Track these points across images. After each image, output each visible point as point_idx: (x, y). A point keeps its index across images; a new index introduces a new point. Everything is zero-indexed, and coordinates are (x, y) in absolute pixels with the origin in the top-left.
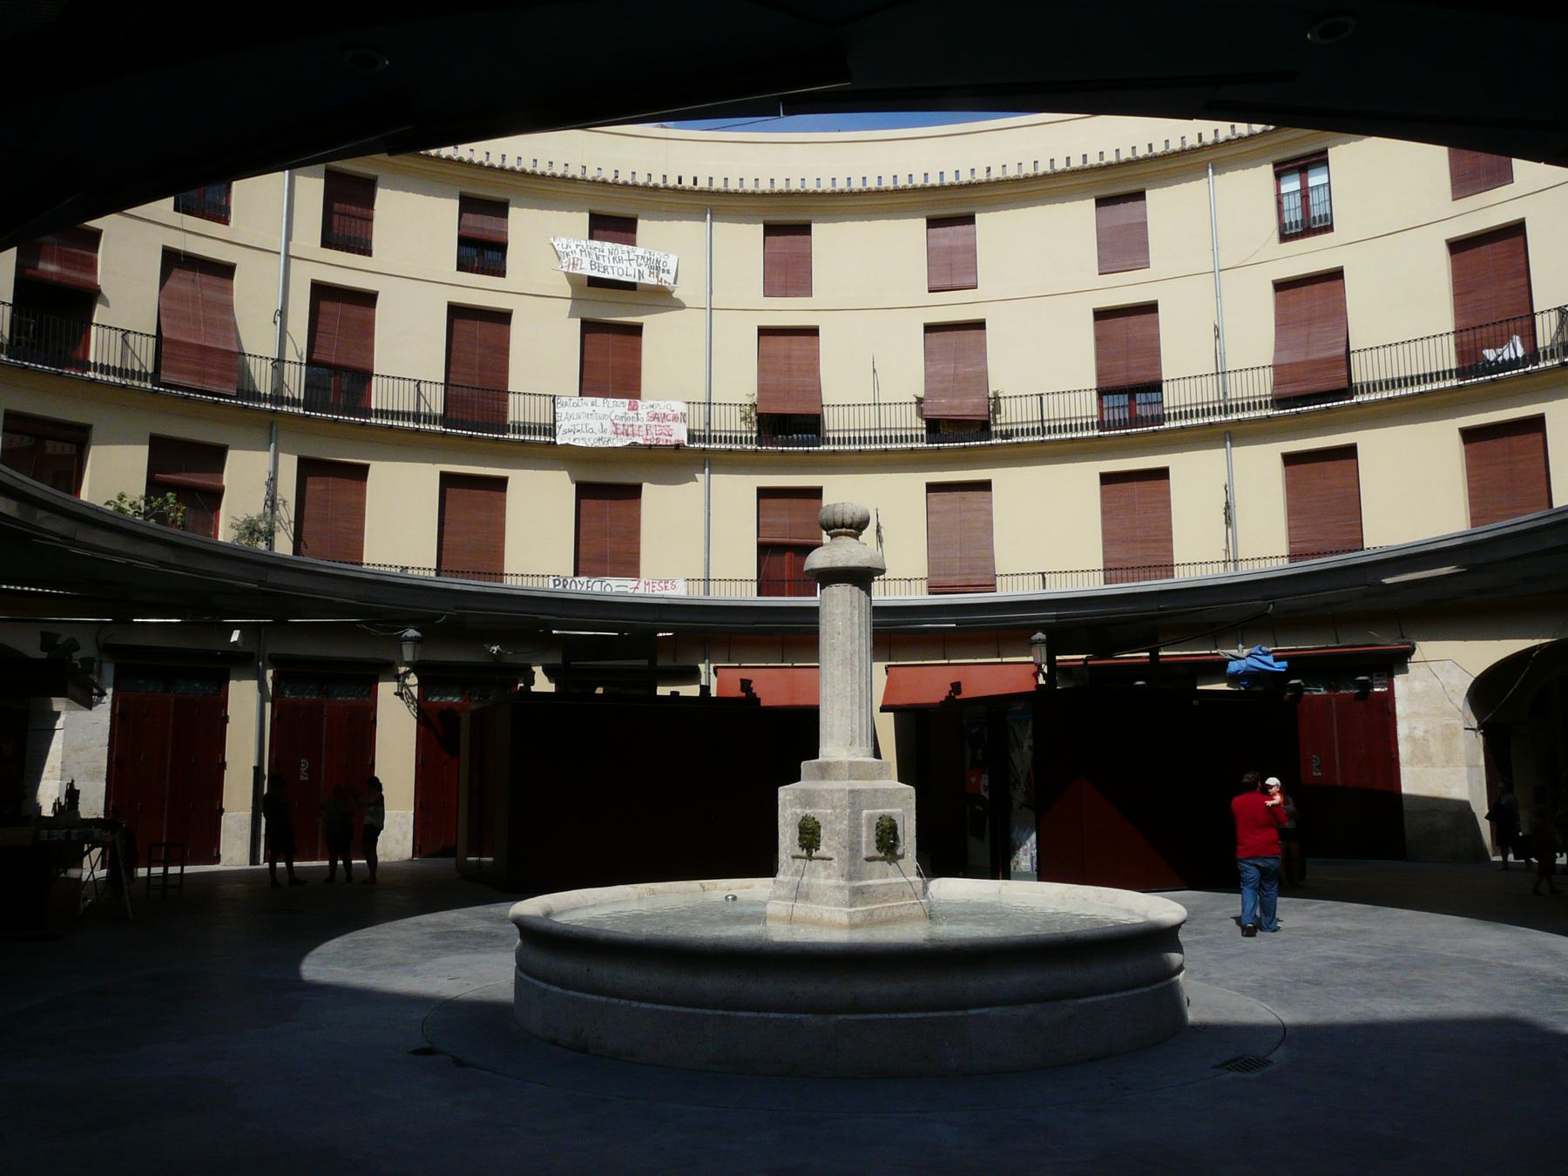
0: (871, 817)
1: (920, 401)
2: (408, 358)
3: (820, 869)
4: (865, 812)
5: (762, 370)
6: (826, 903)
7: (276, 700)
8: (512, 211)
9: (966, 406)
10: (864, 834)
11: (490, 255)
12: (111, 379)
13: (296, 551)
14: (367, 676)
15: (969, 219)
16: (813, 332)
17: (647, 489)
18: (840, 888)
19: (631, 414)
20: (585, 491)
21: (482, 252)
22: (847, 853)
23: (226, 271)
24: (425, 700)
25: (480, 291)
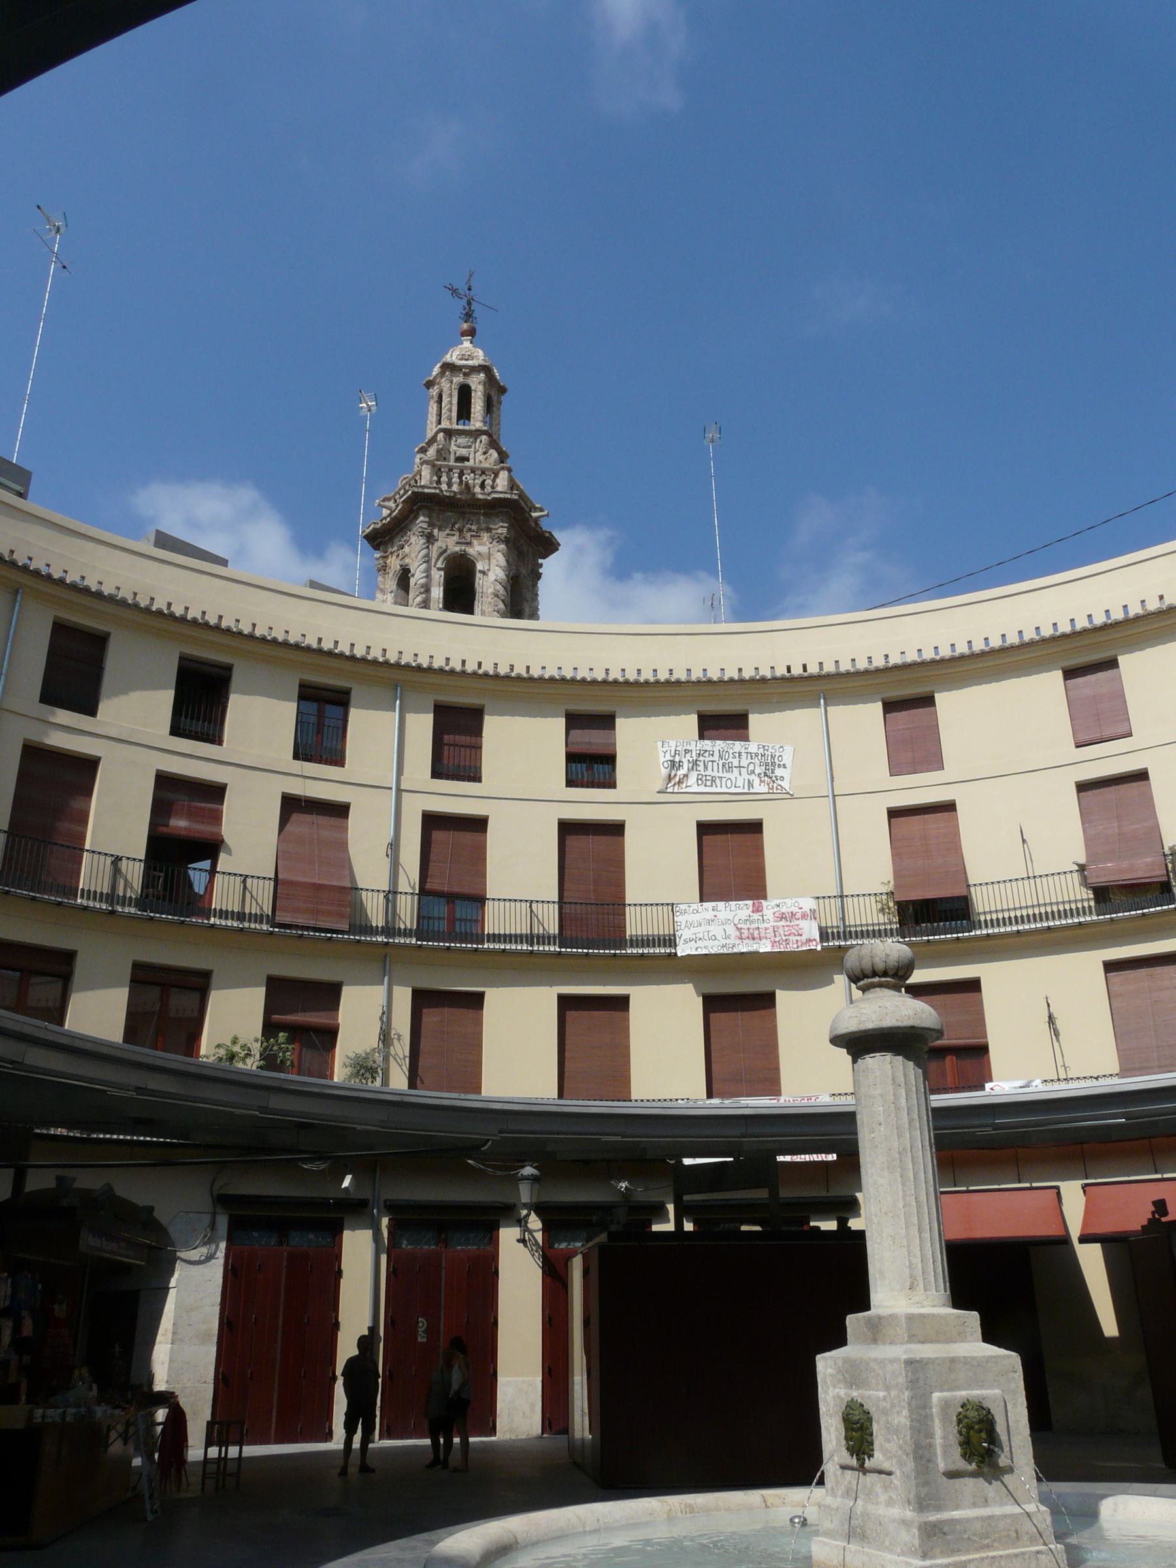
0: (946, 1405)
1: (1082, 868)
2: (521, 879)
3: (878, 1488)
4: (936, 1396)
5: (896, 854)
6: (891, 1551)
7: (392, 1250)
8: (619, 722)
9: (1143, 867)
10: (938, 1433)
11: (599, 768)
12: (229, 923)
13: (412, 1085)
14: (487, 1221)
15: (1112, 664)
16: (949, 807)
17: (781, 996)
18: (904, 1522)
19: (756, 916)
20: (713, 1004)
21: (591, 765)
22: (911, 1465)
23: (340, 810)
24: (551, 1247)
25: (591, 805)
